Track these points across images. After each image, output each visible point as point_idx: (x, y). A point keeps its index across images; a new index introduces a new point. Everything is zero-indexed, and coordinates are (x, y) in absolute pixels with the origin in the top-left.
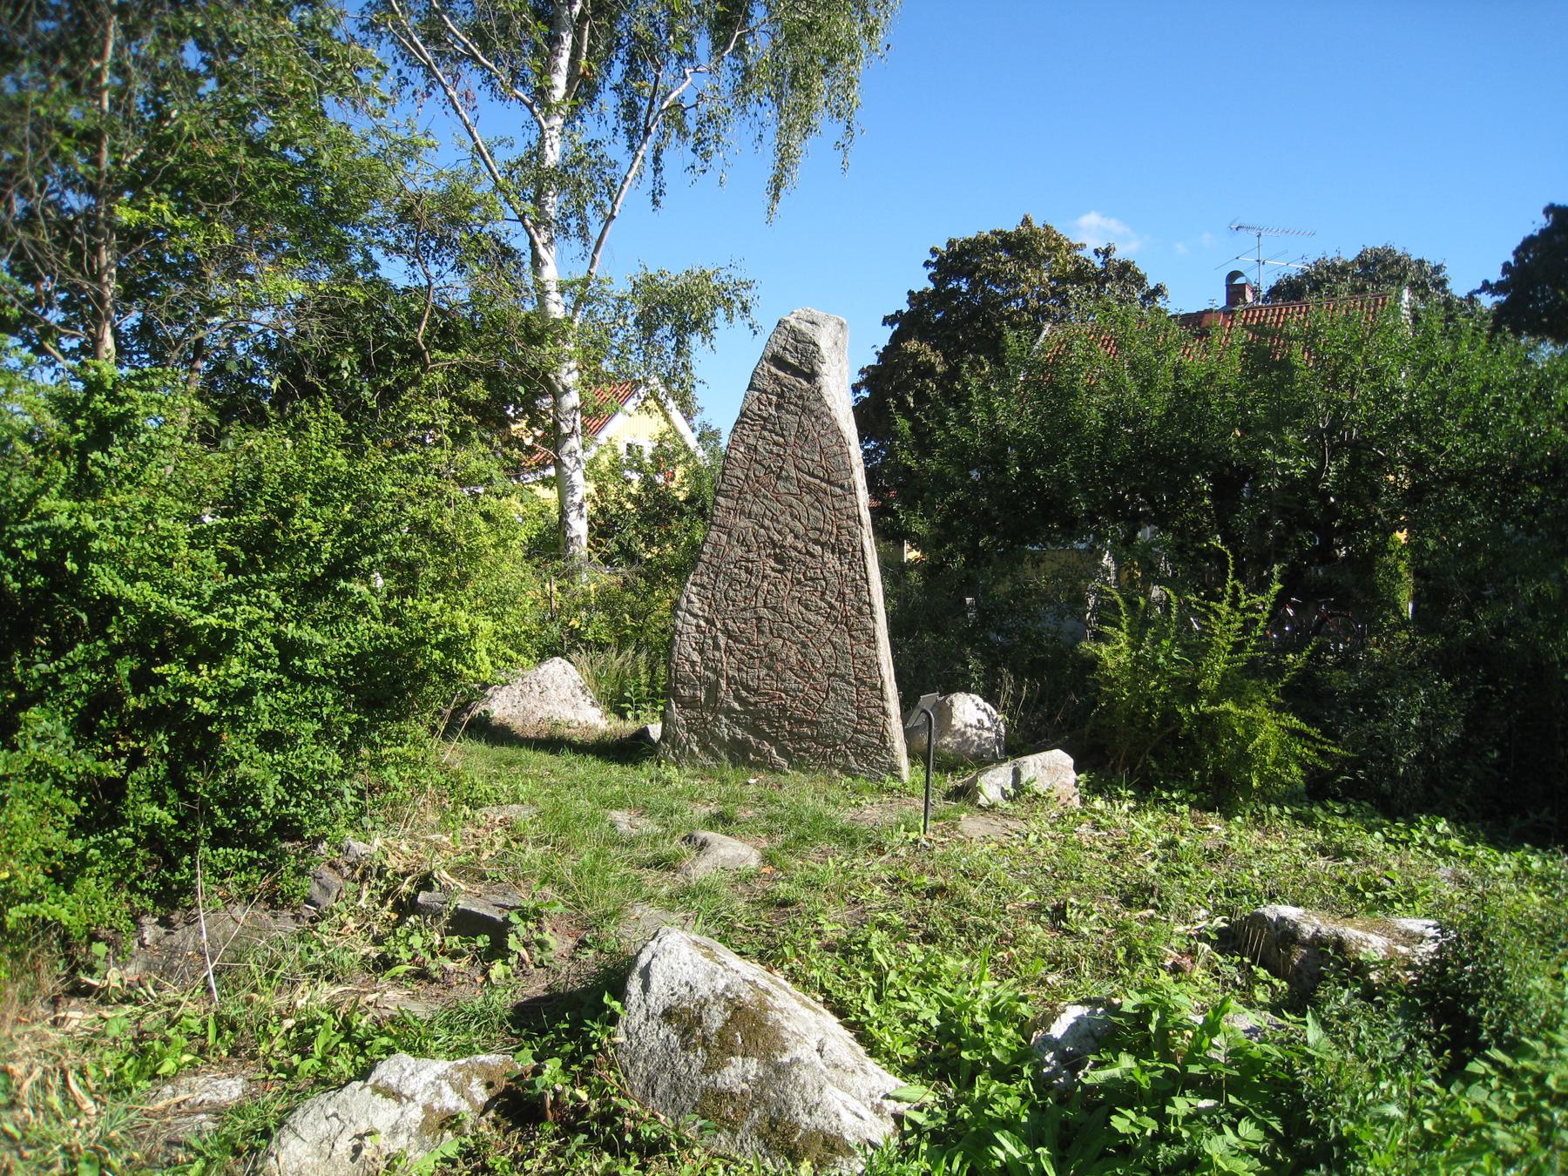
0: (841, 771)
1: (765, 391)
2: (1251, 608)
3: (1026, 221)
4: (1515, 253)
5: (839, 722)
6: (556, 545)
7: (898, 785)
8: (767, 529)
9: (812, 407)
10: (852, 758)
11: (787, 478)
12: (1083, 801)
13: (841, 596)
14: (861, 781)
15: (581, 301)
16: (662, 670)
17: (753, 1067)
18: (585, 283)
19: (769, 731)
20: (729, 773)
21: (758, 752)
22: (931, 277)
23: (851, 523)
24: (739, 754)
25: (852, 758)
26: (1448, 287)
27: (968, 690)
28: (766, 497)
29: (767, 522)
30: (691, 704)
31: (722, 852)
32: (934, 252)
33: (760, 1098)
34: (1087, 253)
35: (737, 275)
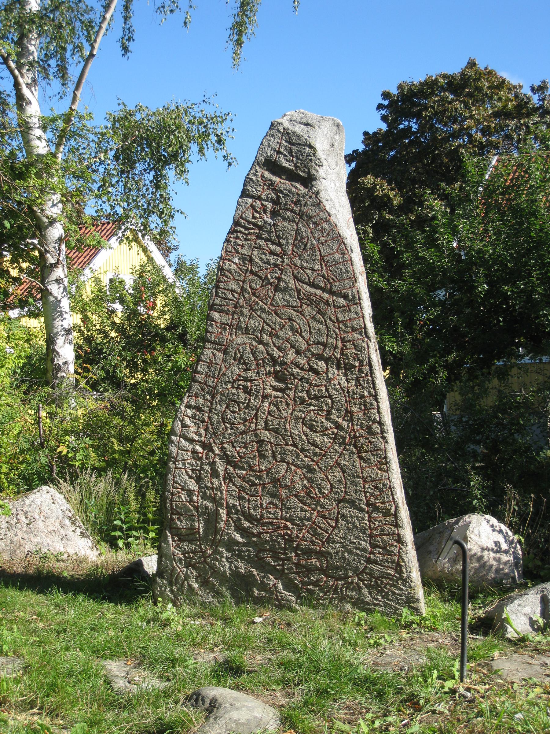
0: (354, 605)
1: (259, 198)
3: (472, 64)
5: (350, 552)
6: (45, 372)
7: (416, 618)
8: (266, 345)
9: (310, 212)
10: (365, 591)
11: (286, 290)
13: (349, 415)
14: (377, 617)
15: (62, 137)
16: (151, 495)
18: (67, 120)
19: (276, 564)
20: (232, 611)
21: (263, 587)
22: (384, 118)
23: (357, 336)
24: (242, 589)
25: (365, 591)
27: (473, 510)
28: (263, 310)
29: (265, 338)
30: (187, 536)
31: (235, 715)
32: (386, 95)
35: (209, 110)
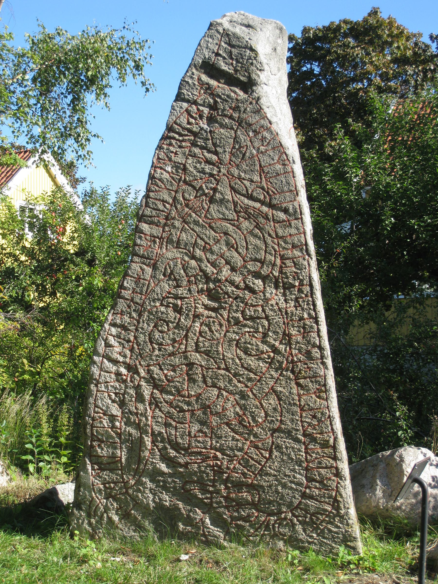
1: (195, 103)
5: (284, 486)
9: (250, 121)
10: (299, 528)
11: (222, 201)
13: (287, 338)
14: (312, 555)
21: (189, 521)
23: (297, 253)
24: (167, 523)
25: (299, 528)
28: (196, 223)
29: (198, 253)
30: (108, 465)
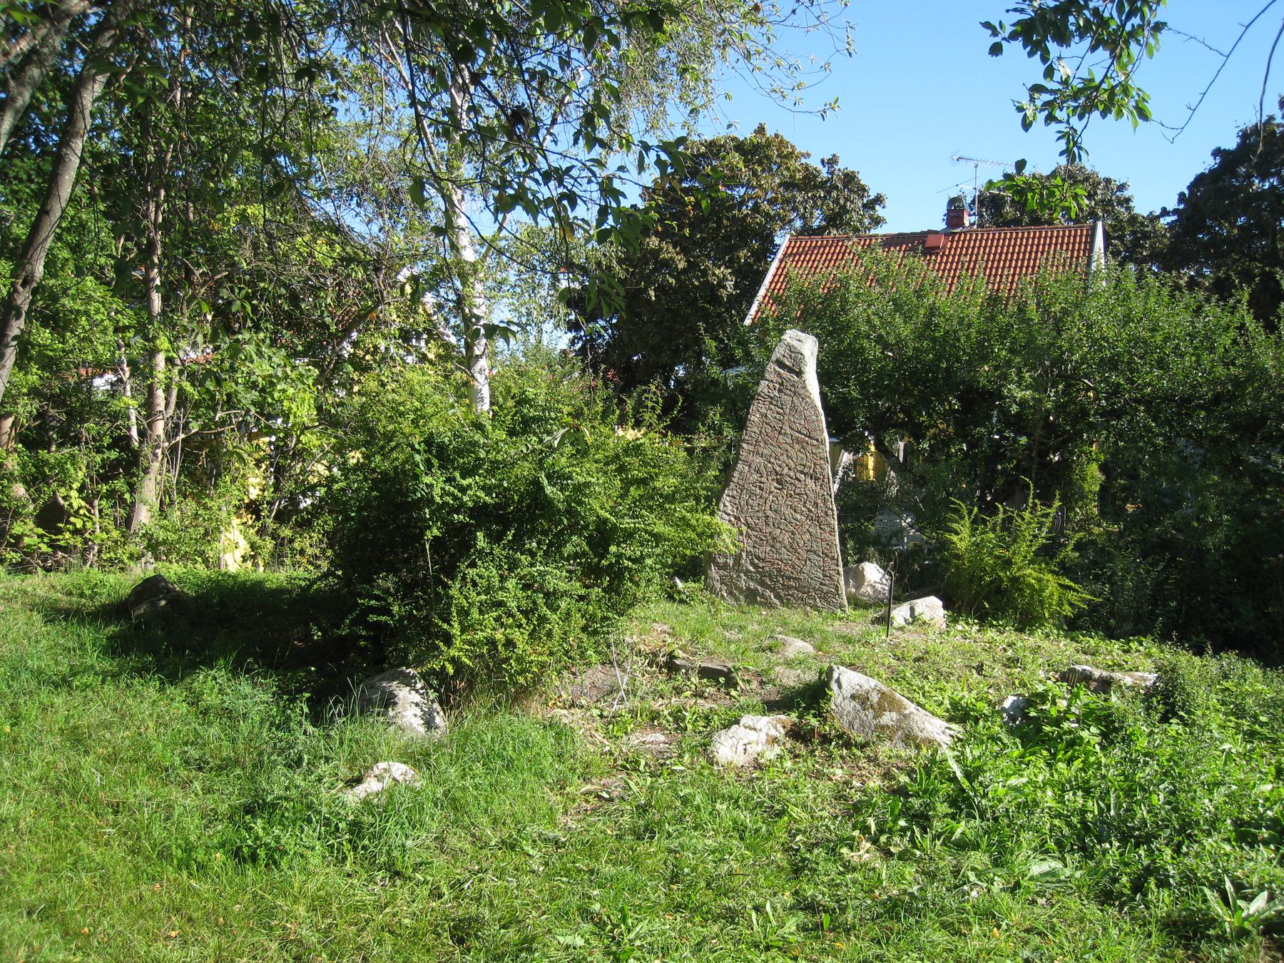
2: (1043, 516)
3: (761, 130)
4: (1189, 188)
12: (948, 626)
17: (894, 715)
21: (763, 596)
24: (751, 596)
26: (1131, 204)
33: (899, 728)
34: (814, 162)
